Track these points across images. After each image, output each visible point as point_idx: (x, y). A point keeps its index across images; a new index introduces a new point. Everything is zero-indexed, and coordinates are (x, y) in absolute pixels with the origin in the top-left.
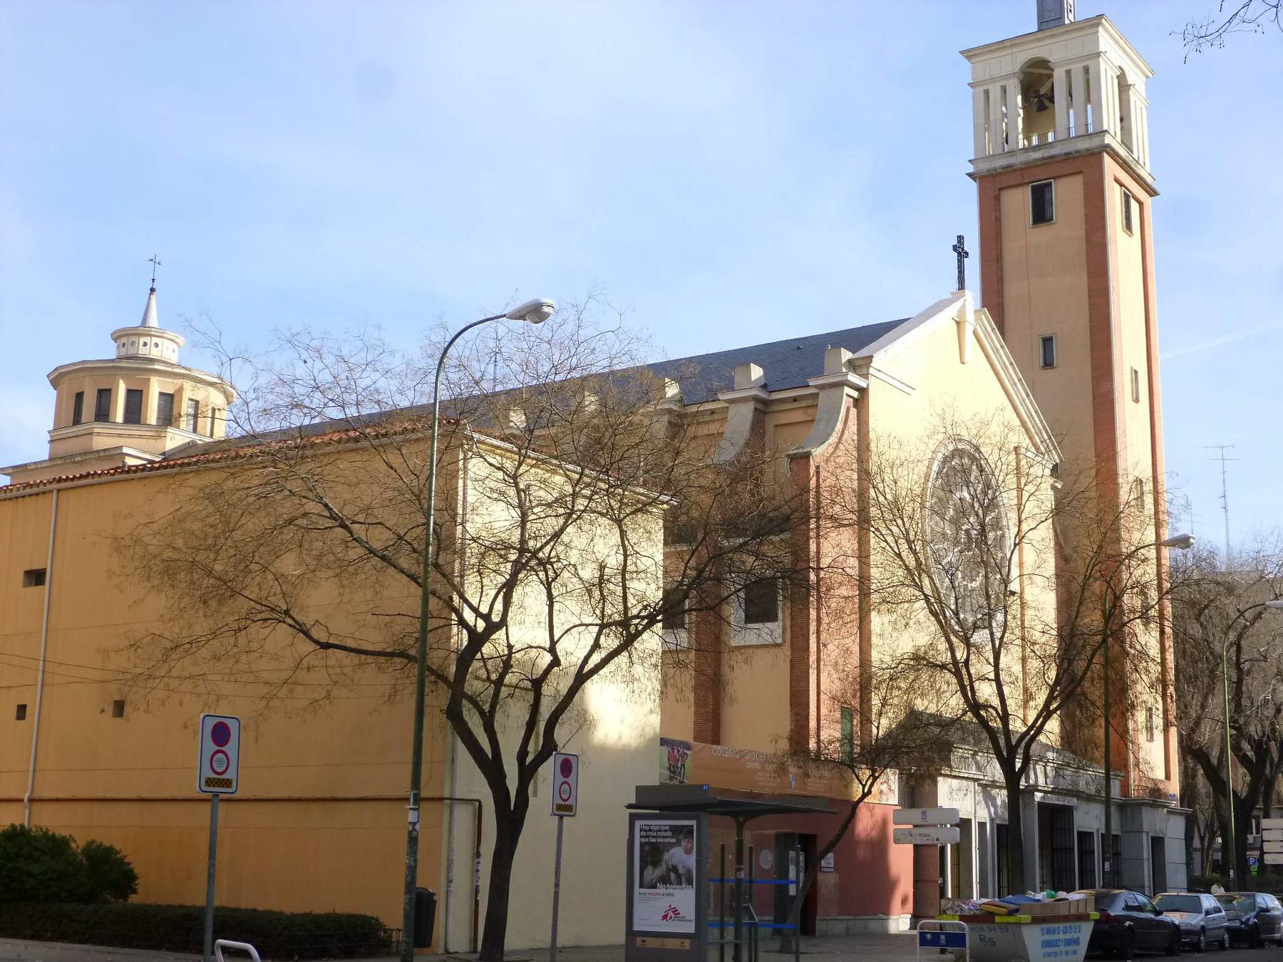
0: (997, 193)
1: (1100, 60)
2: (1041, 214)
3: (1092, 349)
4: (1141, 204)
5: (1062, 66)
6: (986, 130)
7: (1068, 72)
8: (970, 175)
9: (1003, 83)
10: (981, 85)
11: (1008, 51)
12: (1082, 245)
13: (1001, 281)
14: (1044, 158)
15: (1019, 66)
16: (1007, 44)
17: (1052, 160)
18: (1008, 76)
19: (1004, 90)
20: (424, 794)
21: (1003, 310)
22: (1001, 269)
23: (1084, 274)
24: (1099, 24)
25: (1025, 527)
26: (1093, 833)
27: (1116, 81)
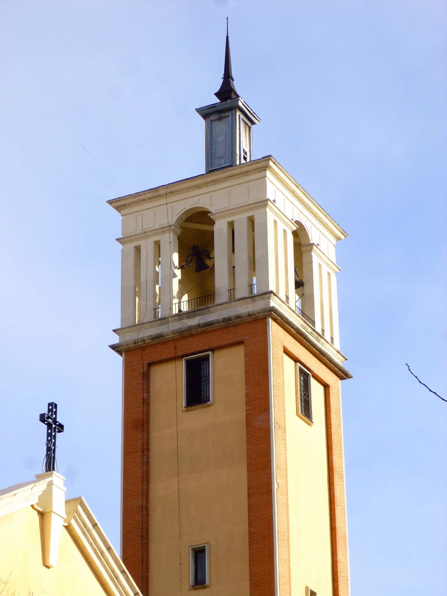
0: (145, 369)
1: (267, 209)
3: (252, 562)
4: (326, 387)
5: (223, 217)
6: (135, 294)
7: (231, 224)
9: (156, 238)
10: (132, 241)
11: (163, 201)
12: (242, 431)
13: (146, 478)
14: (199, 326)
15: (176, 218)
16: (162, 192)
17: (209, 328)
18: (162, 230)
19: (157, 245)
21: (147, 515)
22: (147, 463)
23: (244, 468)
24: (266, 167)
27: (290, 238)
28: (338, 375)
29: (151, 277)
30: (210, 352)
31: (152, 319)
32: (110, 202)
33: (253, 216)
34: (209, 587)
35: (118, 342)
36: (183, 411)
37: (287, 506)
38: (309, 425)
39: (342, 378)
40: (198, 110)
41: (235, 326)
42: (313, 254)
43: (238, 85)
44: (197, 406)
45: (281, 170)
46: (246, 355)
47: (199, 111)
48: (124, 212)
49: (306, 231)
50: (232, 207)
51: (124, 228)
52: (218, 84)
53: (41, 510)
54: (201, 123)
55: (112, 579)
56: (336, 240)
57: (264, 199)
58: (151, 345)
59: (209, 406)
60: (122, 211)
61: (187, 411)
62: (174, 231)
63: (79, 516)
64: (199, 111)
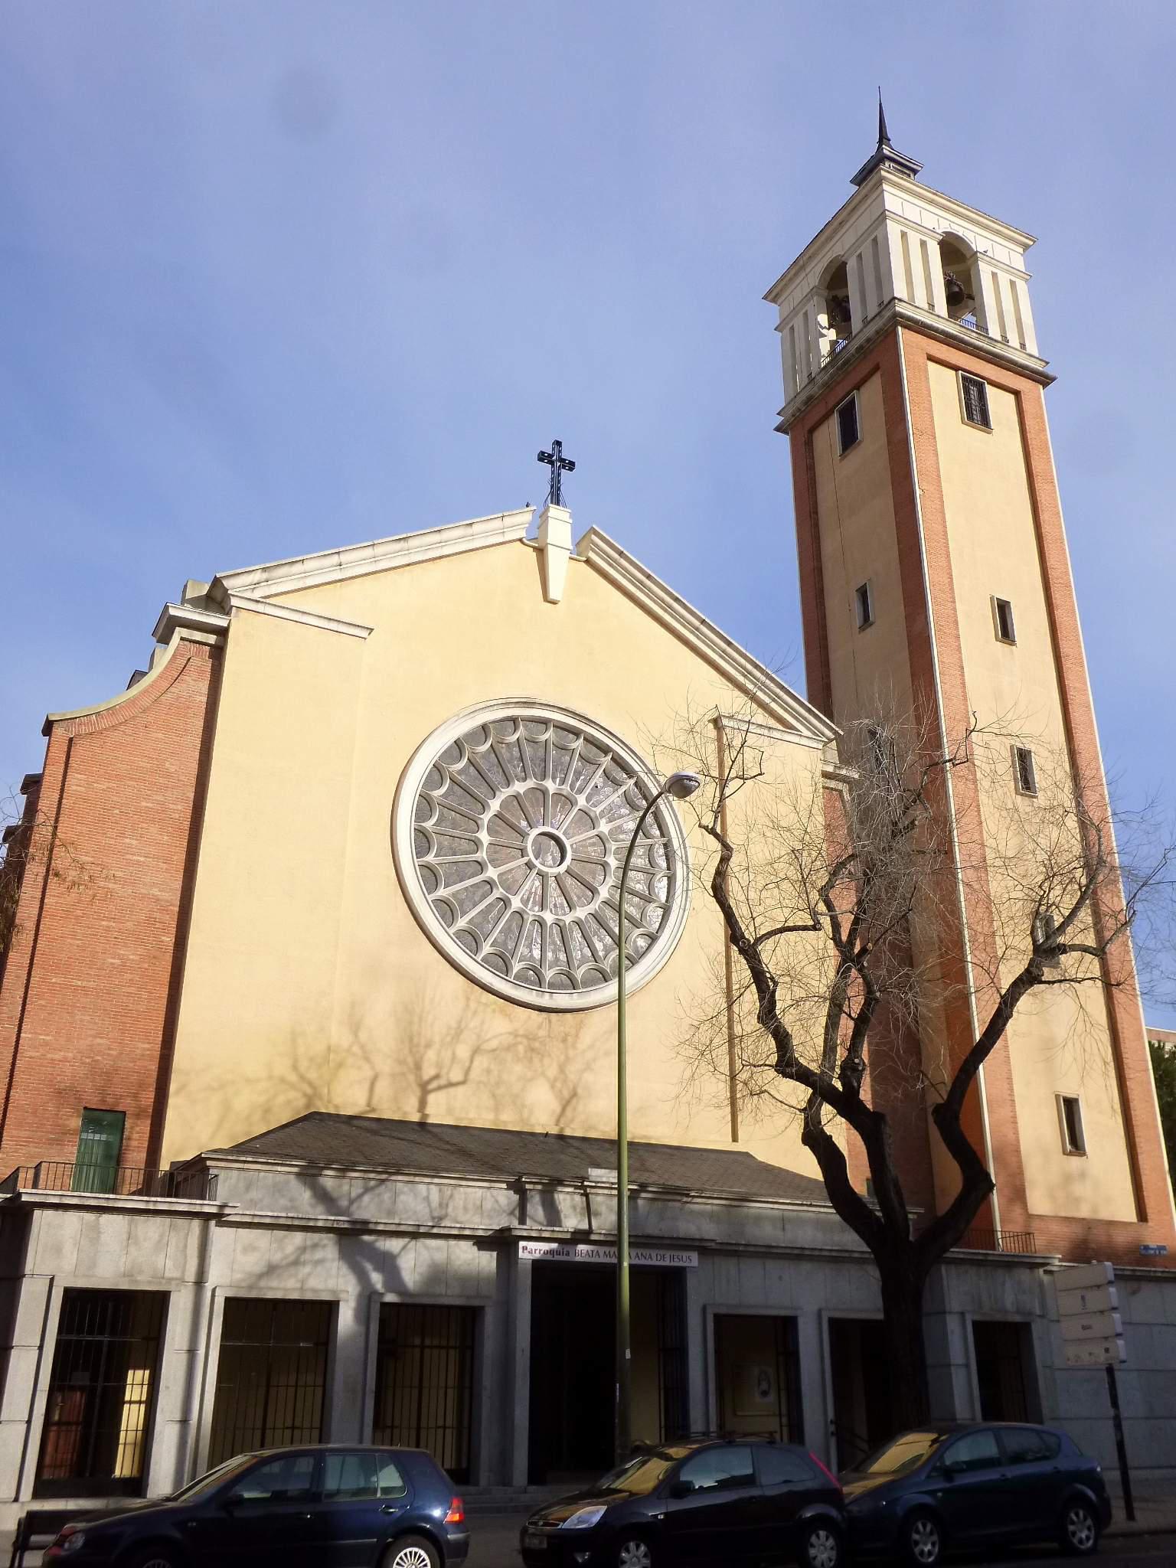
2: (849, 437)
8: (778, 429)
20: (285, 1430)
25: (122, 728)
26: (157, 1303)
39: (1045, 385)
49: (966, 241)
55: (666, 611)
56: (1026, 247)
59: (859, 444)
62: (818, 294)
63: (597, 546)
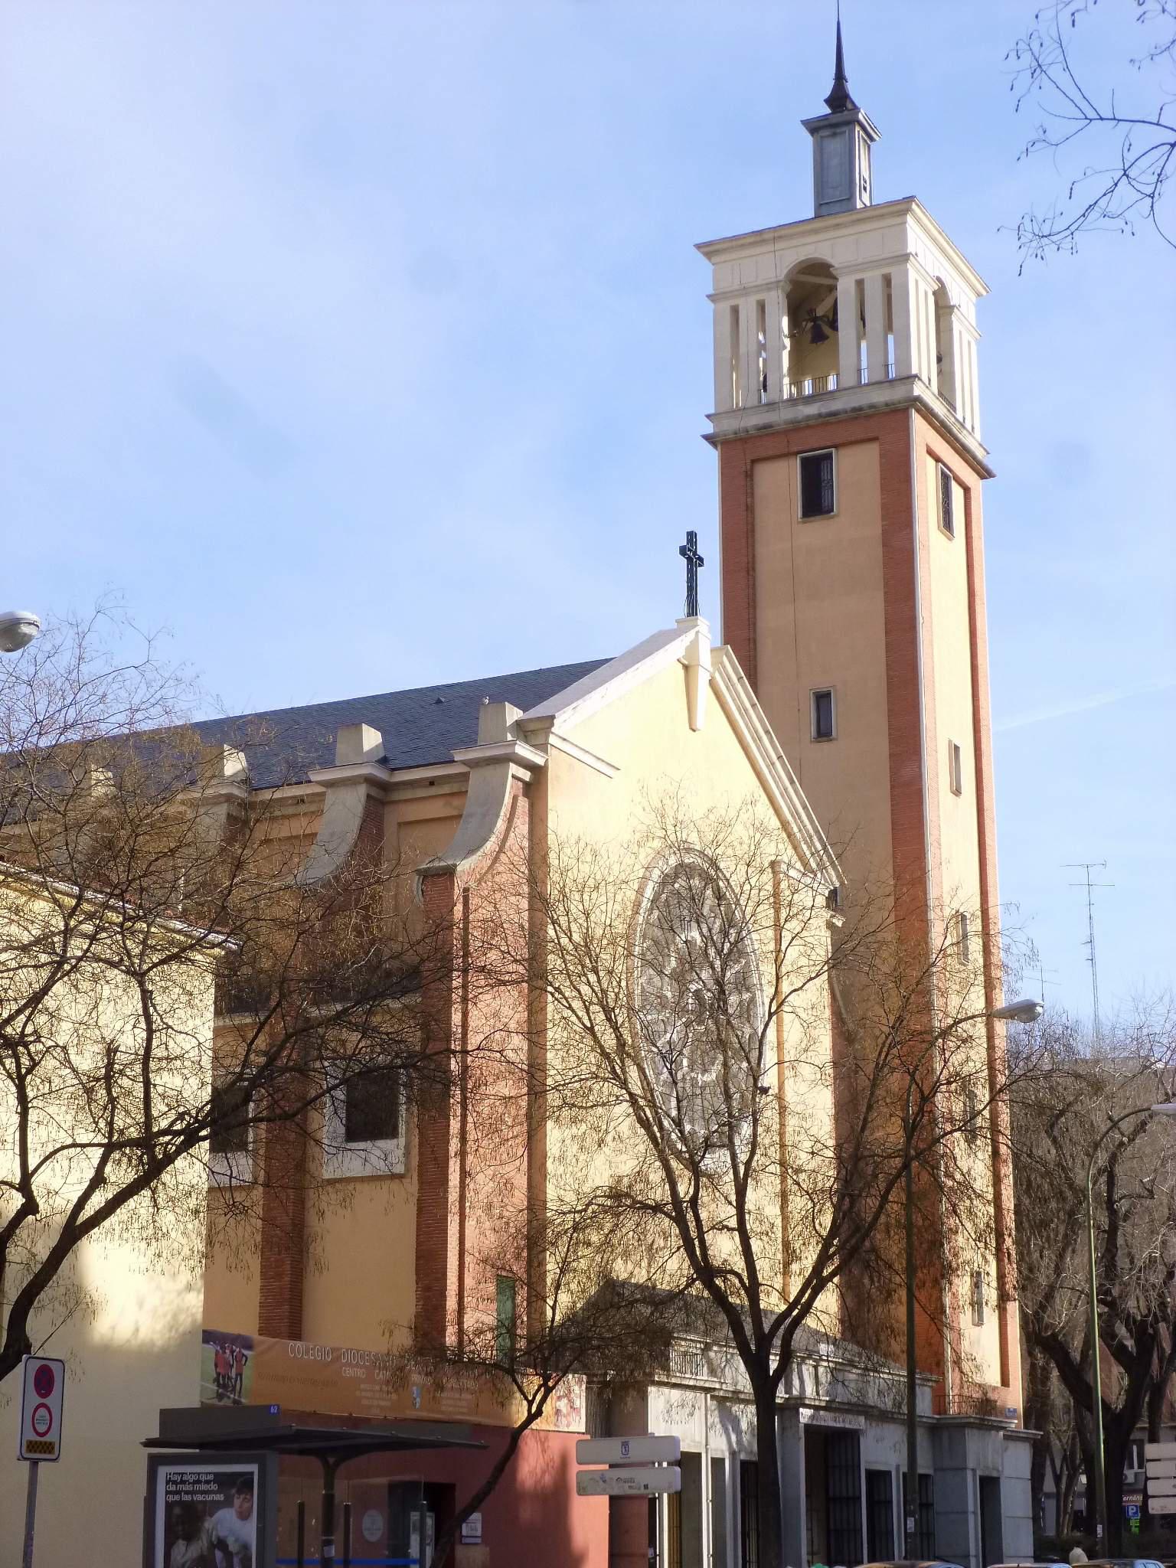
0: (749, 467)
4: (967, 490)
6: (733, 368)
7: (860, 284)
9: (759, 297)
13: (752, 604)
14: (820, 415)
15: (785, 271)
17: (832, 419)
18: (768, 287)
19: (762, 307)
23: (879, 597)
24: (908, 210)
27: (931, 299)
28: (978, 474)
29: (754, 347)
30: (833, 450)
31: (756, 403)
32: (698, 246)
33: (890, 274)
34: (836, 739)
35: (712, 431)
36: (798, 523)
37: (932, 645)
38: (950, 540)
39: (982, 477)
40: (806, 123)
41: (868, 417)
42: (954, 318)
43: (852, 88)
44: (818, 517)
45: (924, 213)
46: (882, 456)
47: (806, 123)
48: (716, 259)
50: (860, 260)
51: (716, 280)
52: (827, 87)
53: (686, 663)
54: (807, 140)
55: (755, 741)
57: (903, 253)
58: (756, 437)
59: (833, 517)
60: (713, 259)
61: (804, 523)
63: (724, 667)
64: (806, 123)
